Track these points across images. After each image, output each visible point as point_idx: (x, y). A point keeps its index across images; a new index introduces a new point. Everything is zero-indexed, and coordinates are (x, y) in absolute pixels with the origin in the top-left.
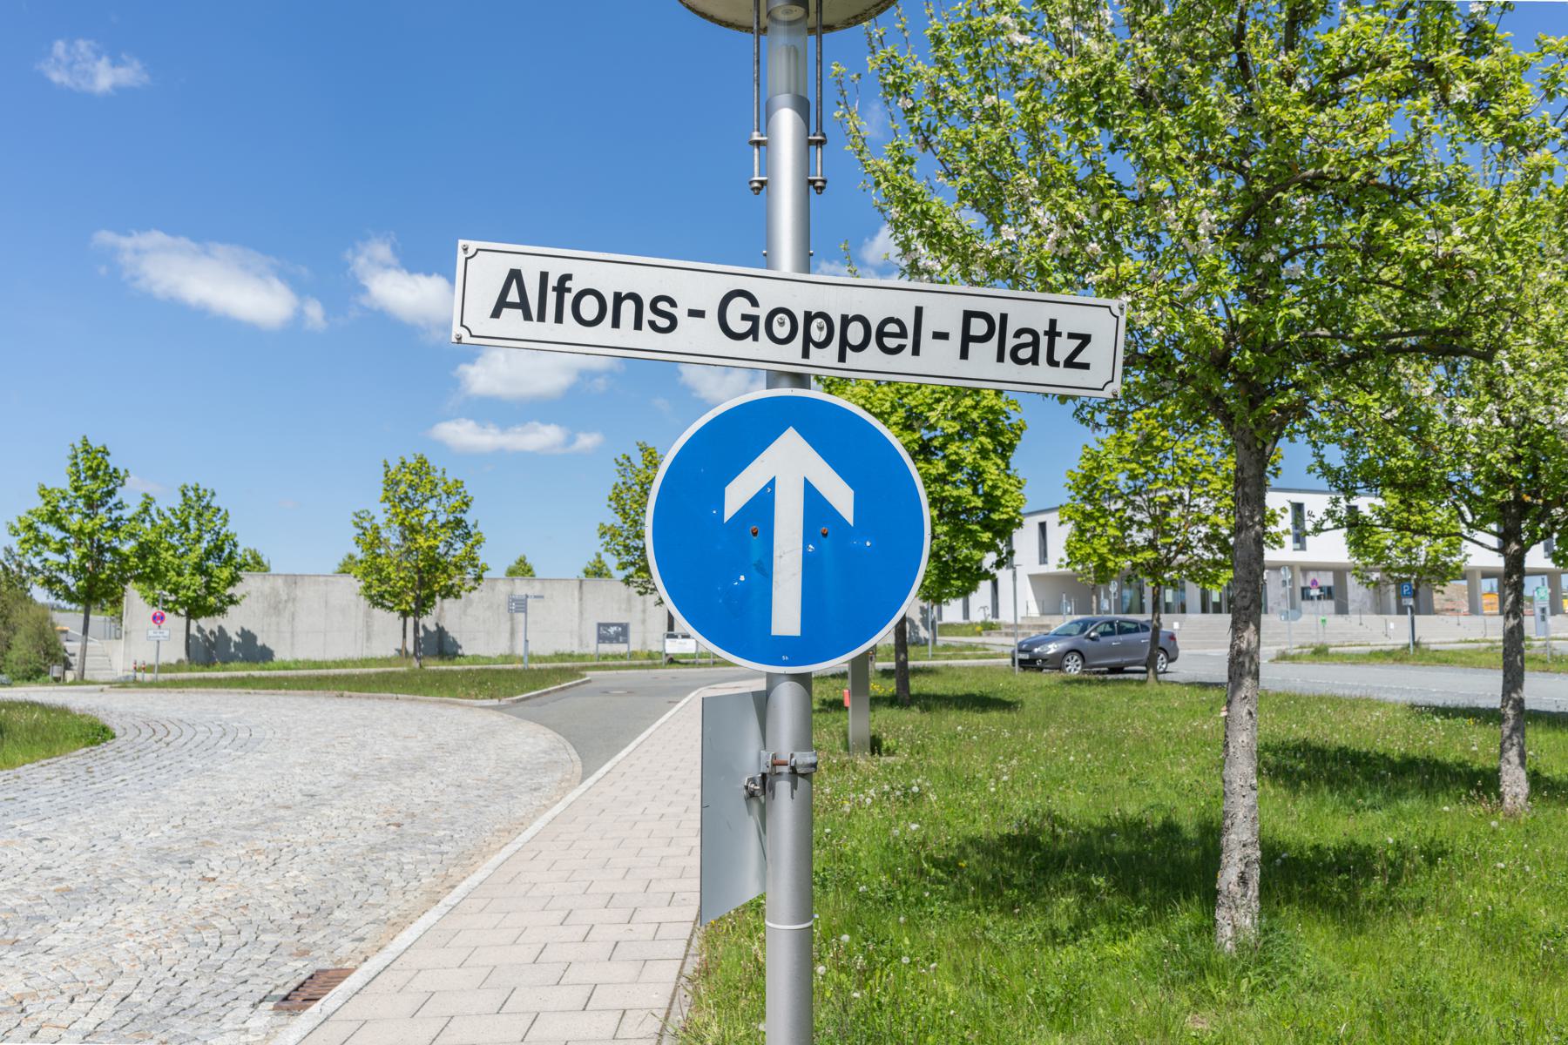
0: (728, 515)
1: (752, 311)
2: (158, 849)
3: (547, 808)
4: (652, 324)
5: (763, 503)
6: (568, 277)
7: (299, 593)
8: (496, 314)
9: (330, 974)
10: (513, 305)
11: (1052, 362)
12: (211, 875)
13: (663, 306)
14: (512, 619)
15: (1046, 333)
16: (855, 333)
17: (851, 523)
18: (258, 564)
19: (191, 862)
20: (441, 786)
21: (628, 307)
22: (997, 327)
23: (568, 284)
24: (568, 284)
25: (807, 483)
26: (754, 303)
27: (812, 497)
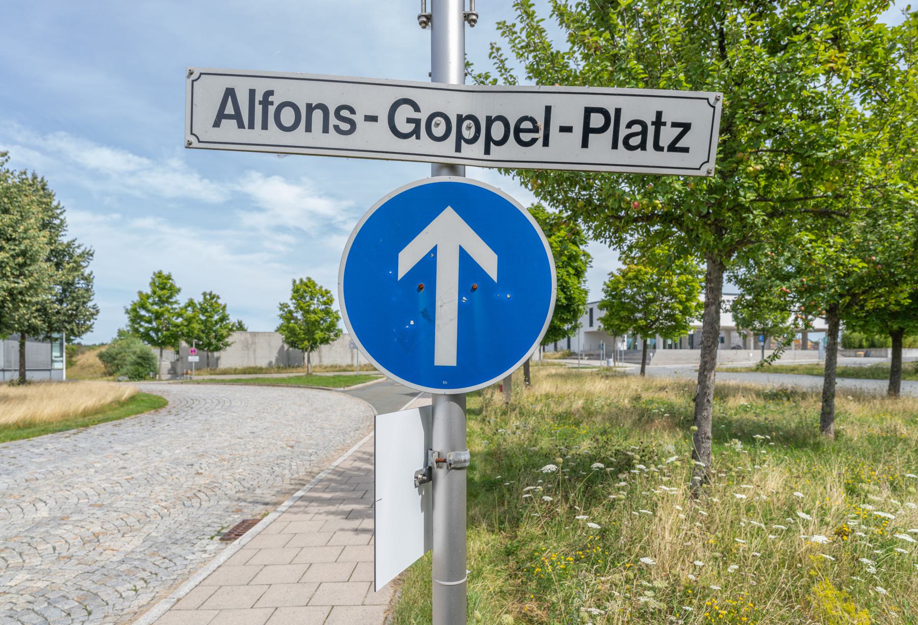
0: (401, 275)
1: (416, 115)
2: (178, 459)
3: (361, 439)
4: (337, 128)
5: (428, 265)
6: (270, 93)
7: (257, 340)
8: (217, 124)
9: (250, 522)
10: (229, 117)
11: (657, 147)
12: (200, 471)
13: (345, 113)
14: (352, 352)
15: (653, 123)
16: (498, 131)
17: (494, 277)
18: (241, 327)
19: (192, 465)
20: (314, 428)
21: (318, 115)
22: (612, 119)
23: (271, 99)
24: (271, 99)
25: (461, 247)
26: (417, 109)
27: (466, 260)
